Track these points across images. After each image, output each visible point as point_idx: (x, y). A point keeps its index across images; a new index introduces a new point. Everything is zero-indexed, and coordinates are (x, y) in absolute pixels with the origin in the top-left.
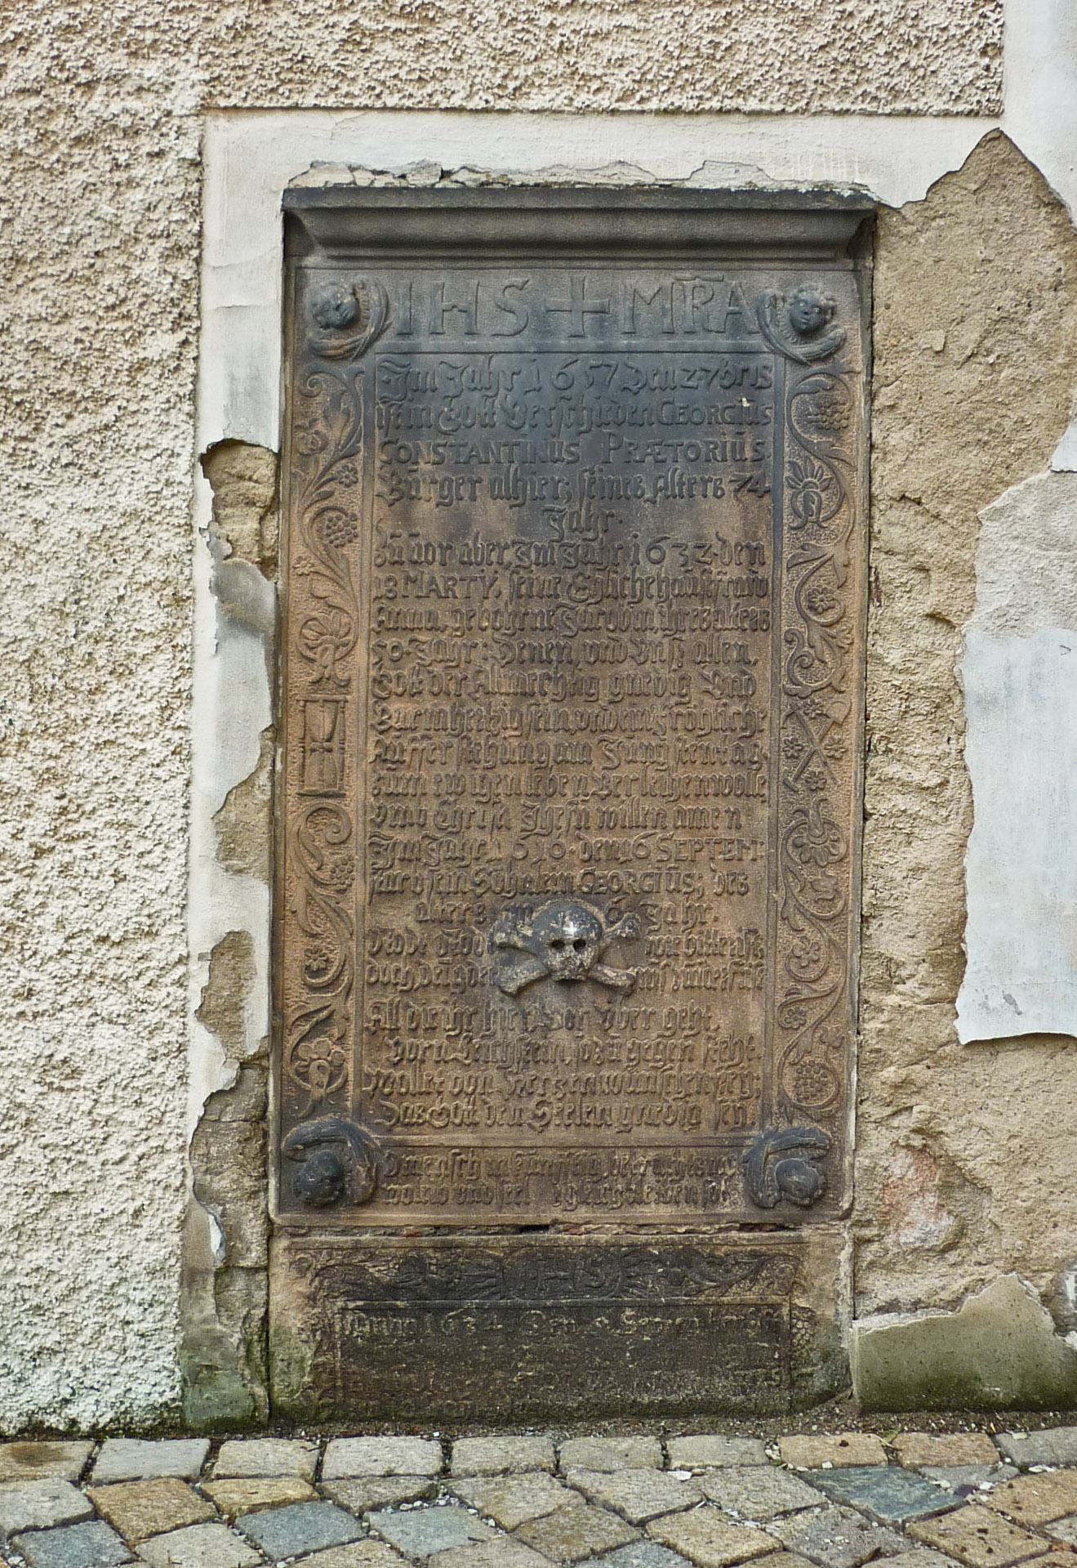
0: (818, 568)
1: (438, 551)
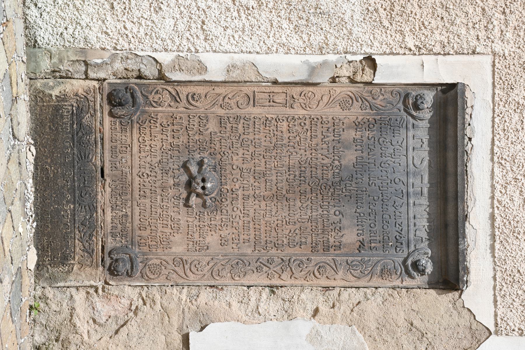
0: (333, 269)
1: (338, 138)
